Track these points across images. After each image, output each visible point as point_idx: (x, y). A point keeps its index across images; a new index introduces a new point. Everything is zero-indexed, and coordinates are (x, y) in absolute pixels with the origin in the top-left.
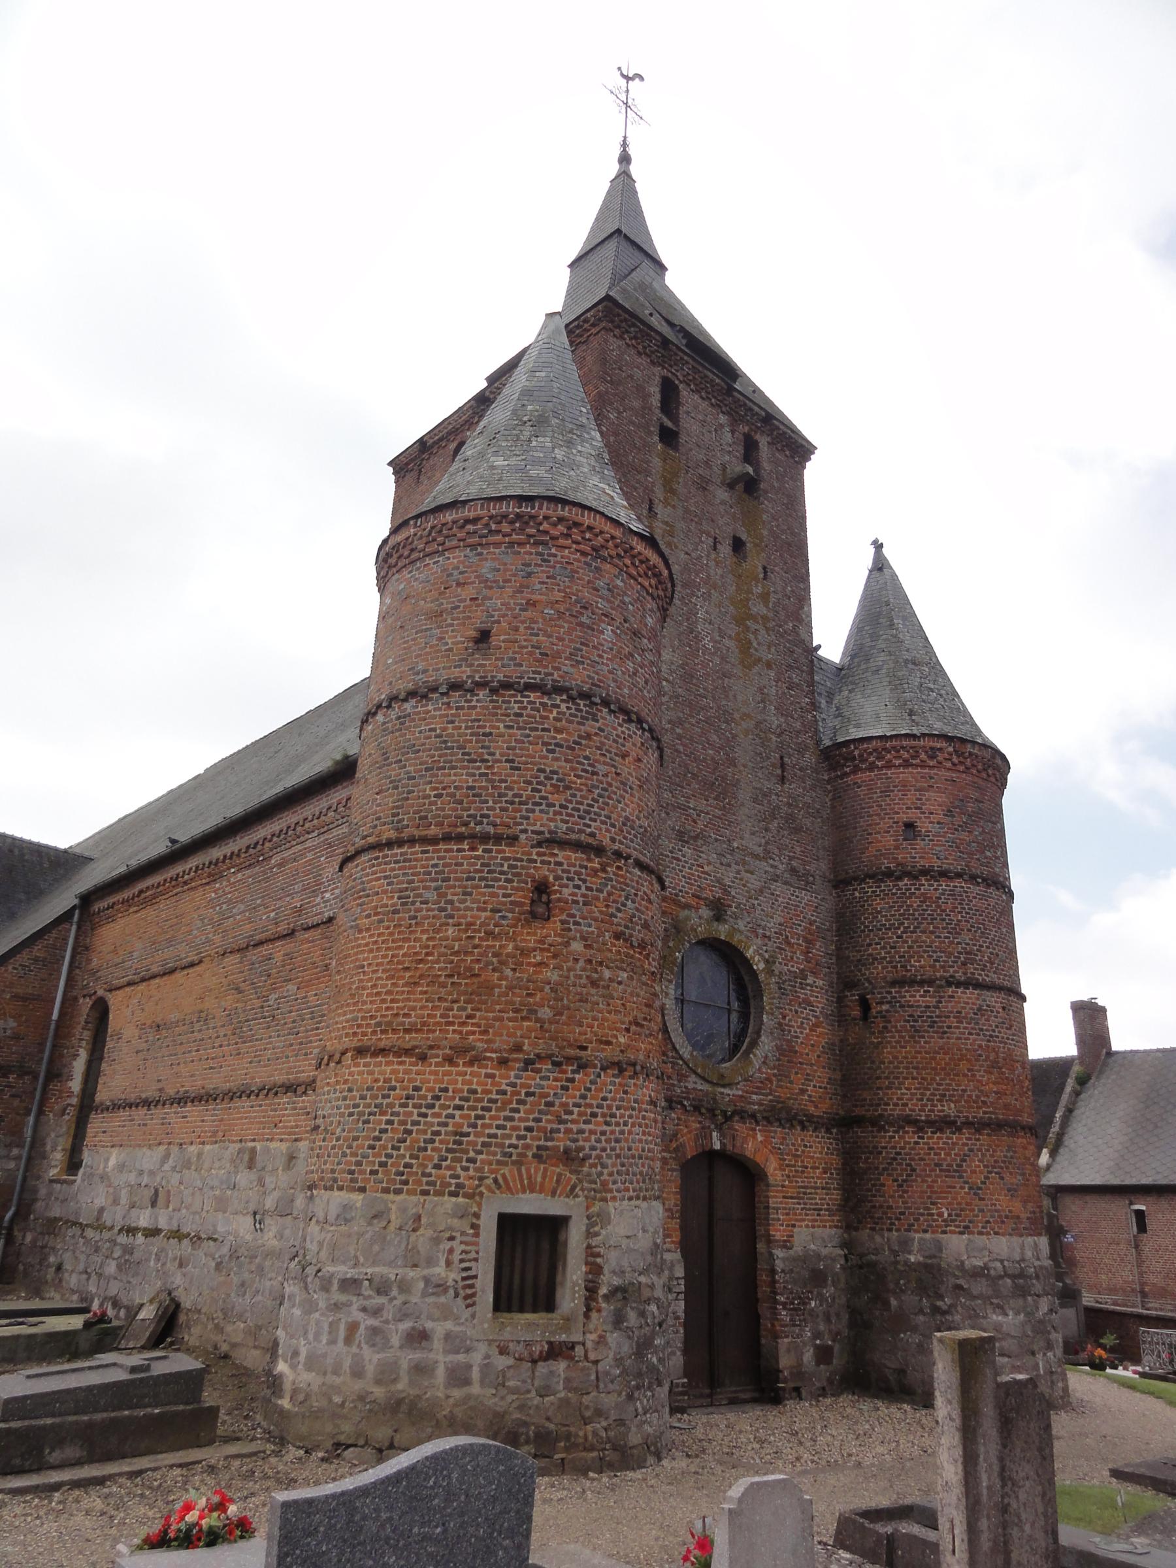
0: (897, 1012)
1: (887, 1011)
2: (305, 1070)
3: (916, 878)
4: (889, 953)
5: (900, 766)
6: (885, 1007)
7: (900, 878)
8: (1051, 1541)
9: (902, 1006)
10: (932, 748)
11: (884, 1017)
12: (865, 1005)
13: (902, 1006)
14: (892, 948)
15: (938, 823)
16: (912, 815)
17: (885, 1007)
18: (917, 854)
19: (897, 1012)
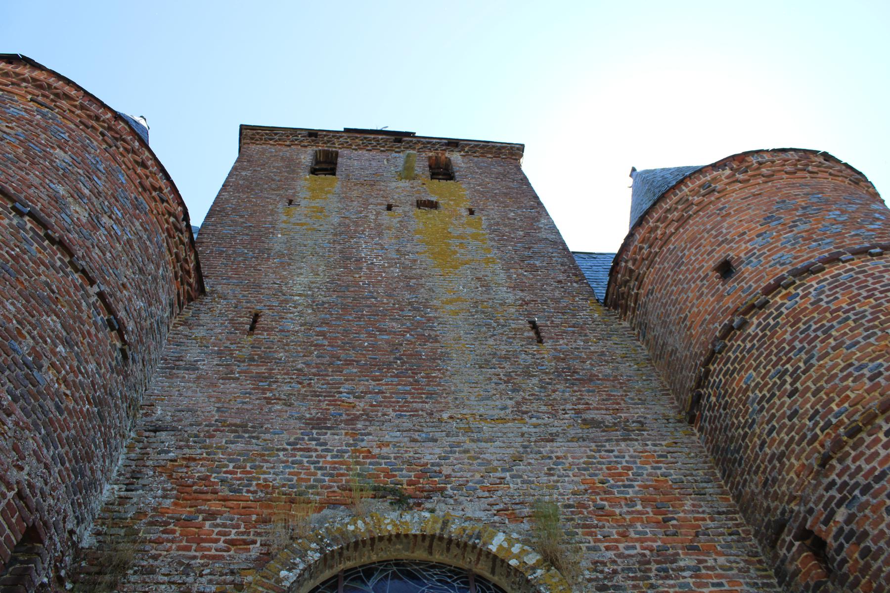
0: (863, 507)
1: (850, 519)
2: (42, 465)
3: (764, 305)
4: (791, 428)
5: (677, 229)
6: (841, 515)
7: (744, 324)
8: (688, 497)
9: (866, 489)
10: (702, 186)
11: (852, 533)
12: (817, 546)
13: (866, 489)
14: (790, 418)
15: (758, 236)
16: (718, 256)
17: (841, 515)
18: (751, 281)
19: (863, 507)
